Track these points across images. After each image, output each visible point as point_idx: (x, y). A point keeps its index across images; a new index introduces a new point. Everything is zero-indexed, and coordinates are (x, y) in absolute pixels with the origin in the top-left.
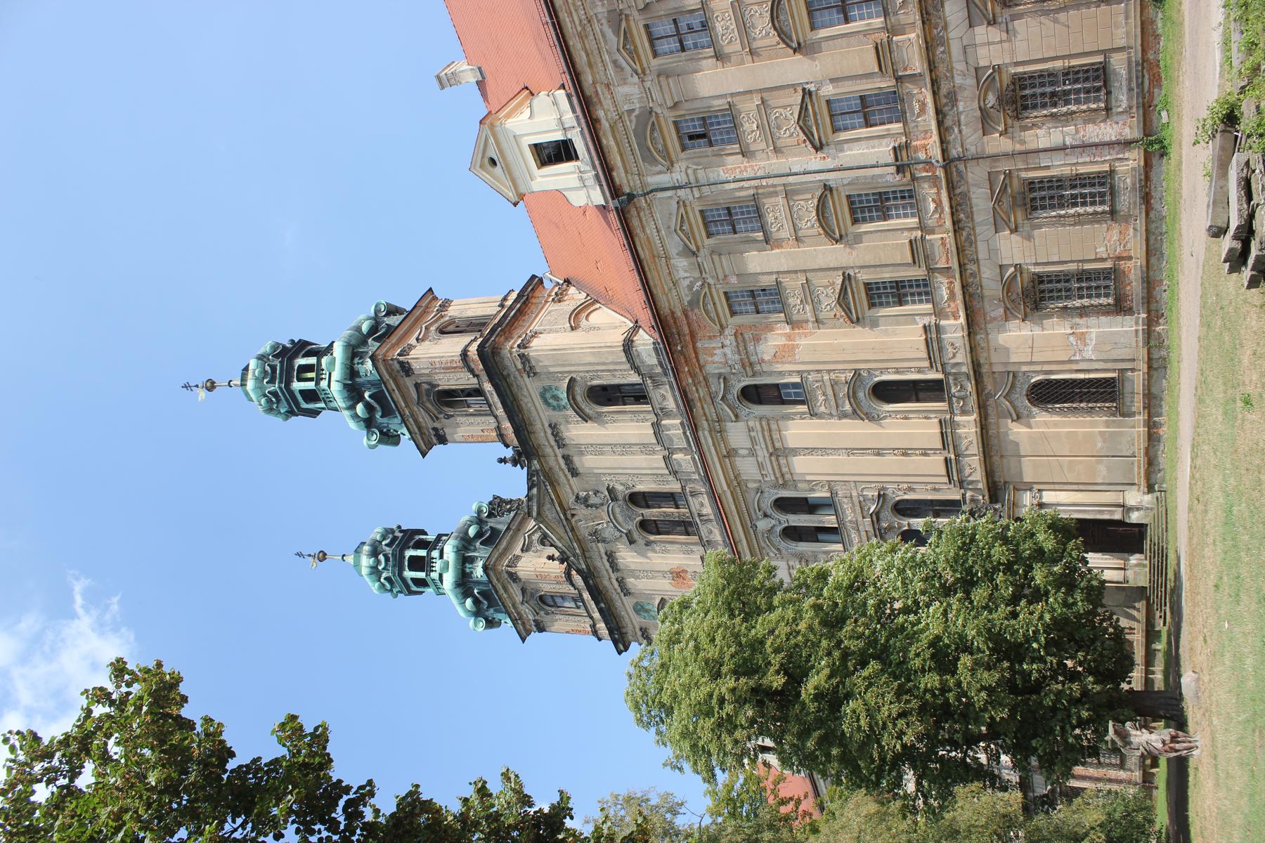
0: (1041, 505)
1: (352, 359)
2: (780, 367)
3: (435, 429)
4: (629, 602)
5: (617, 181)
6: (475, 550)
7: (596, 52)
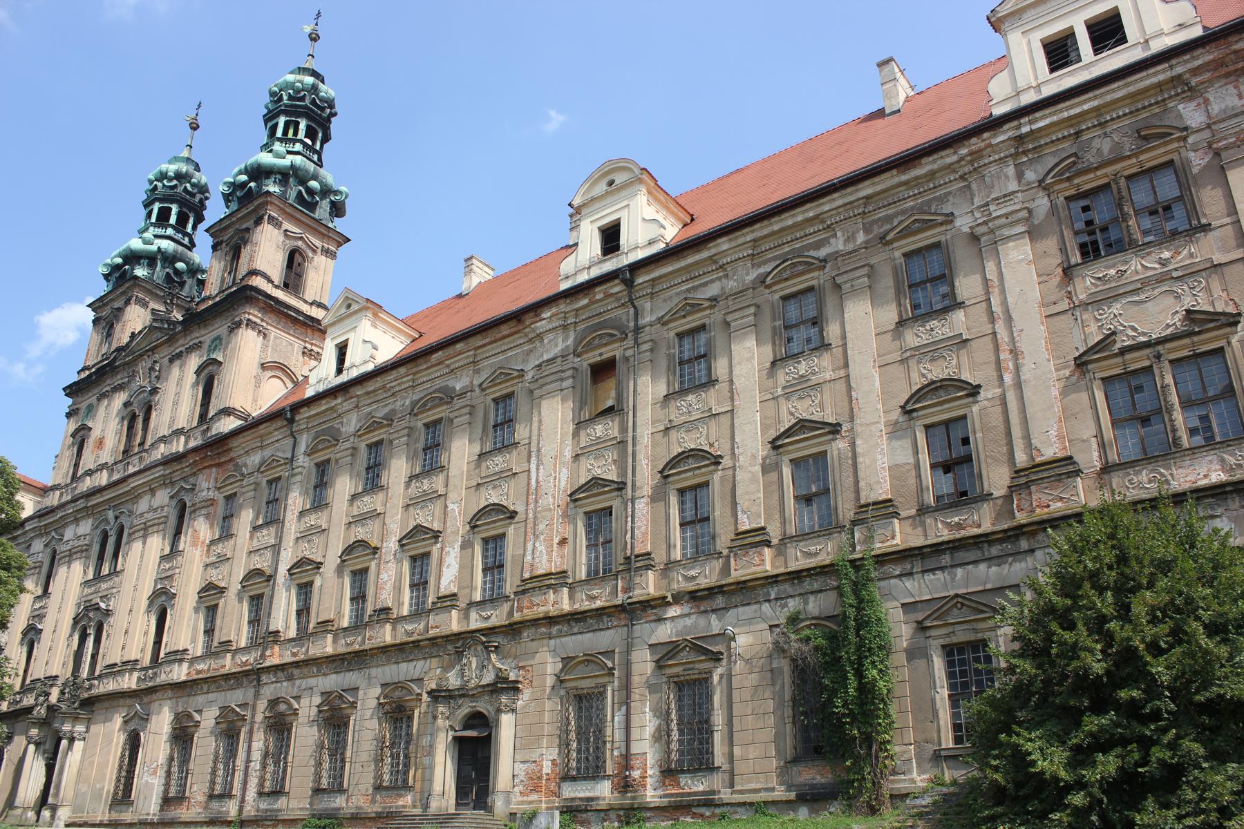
0: (72, 740)
1: (279, 173)
2: (190, 530)
4: (93, 400)
6: (163, 267)
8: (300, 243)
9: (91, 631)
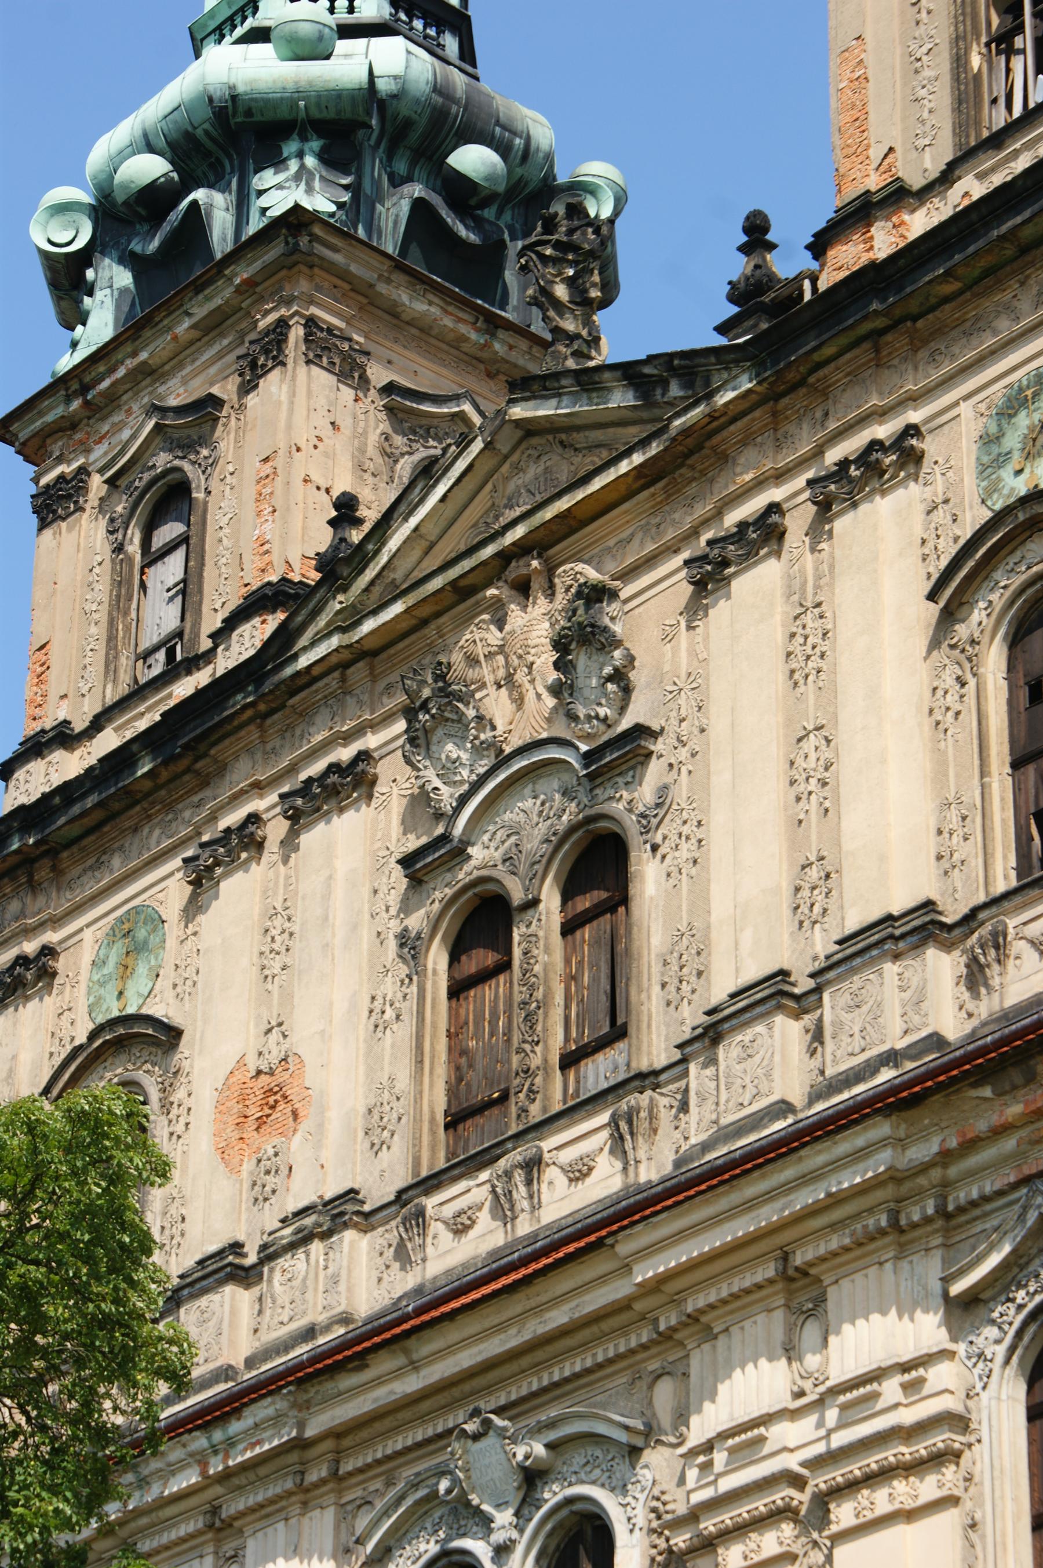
3: (78, 481)
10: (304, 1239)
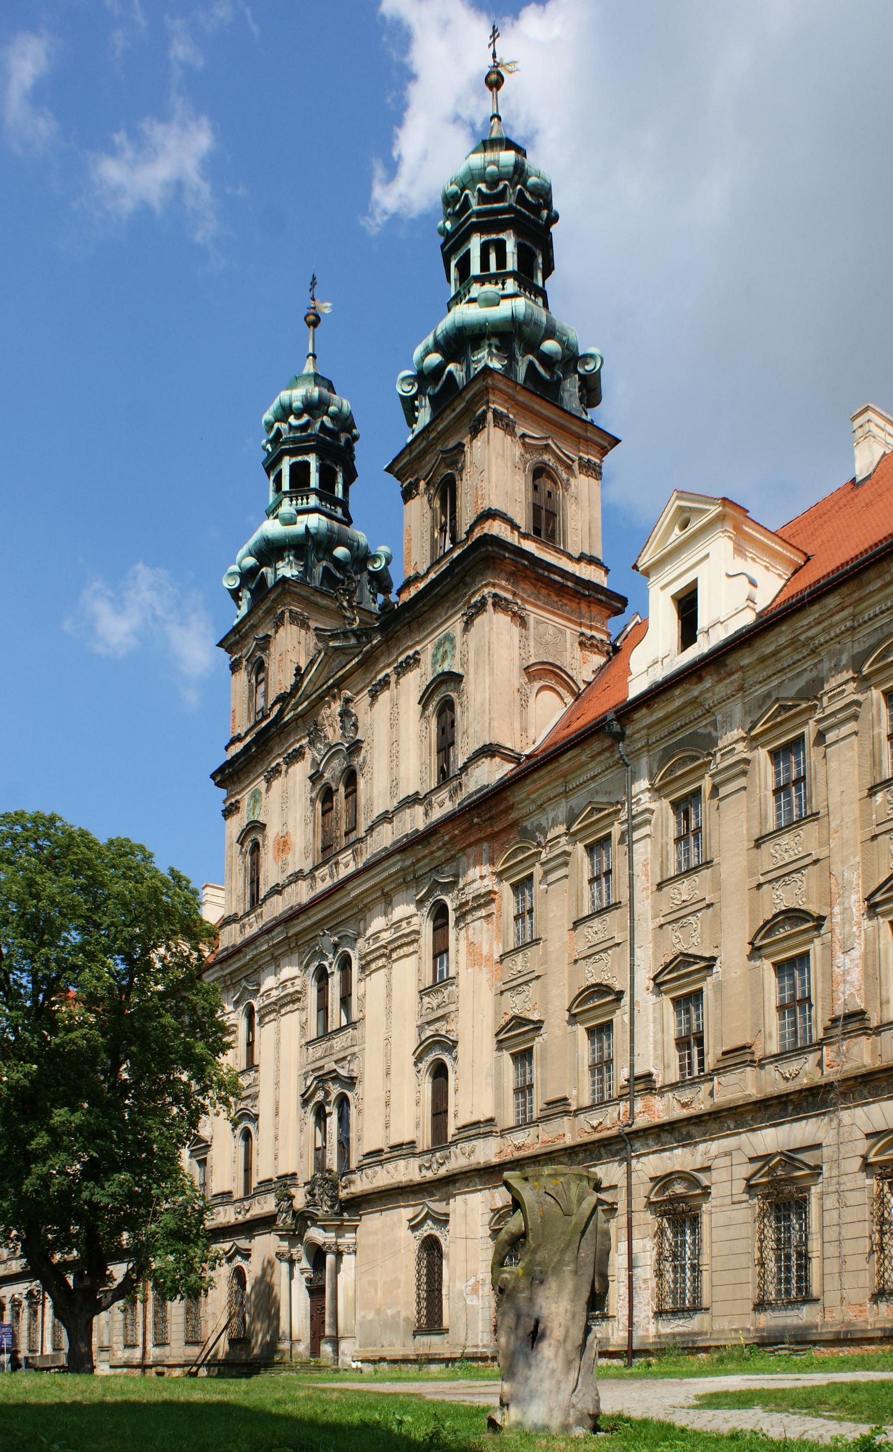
0: (339, 1255)
5: (636, 716)
7: (779, 666)
8: (546, 457)
9: (331, 1108)
10: (290, 883)
